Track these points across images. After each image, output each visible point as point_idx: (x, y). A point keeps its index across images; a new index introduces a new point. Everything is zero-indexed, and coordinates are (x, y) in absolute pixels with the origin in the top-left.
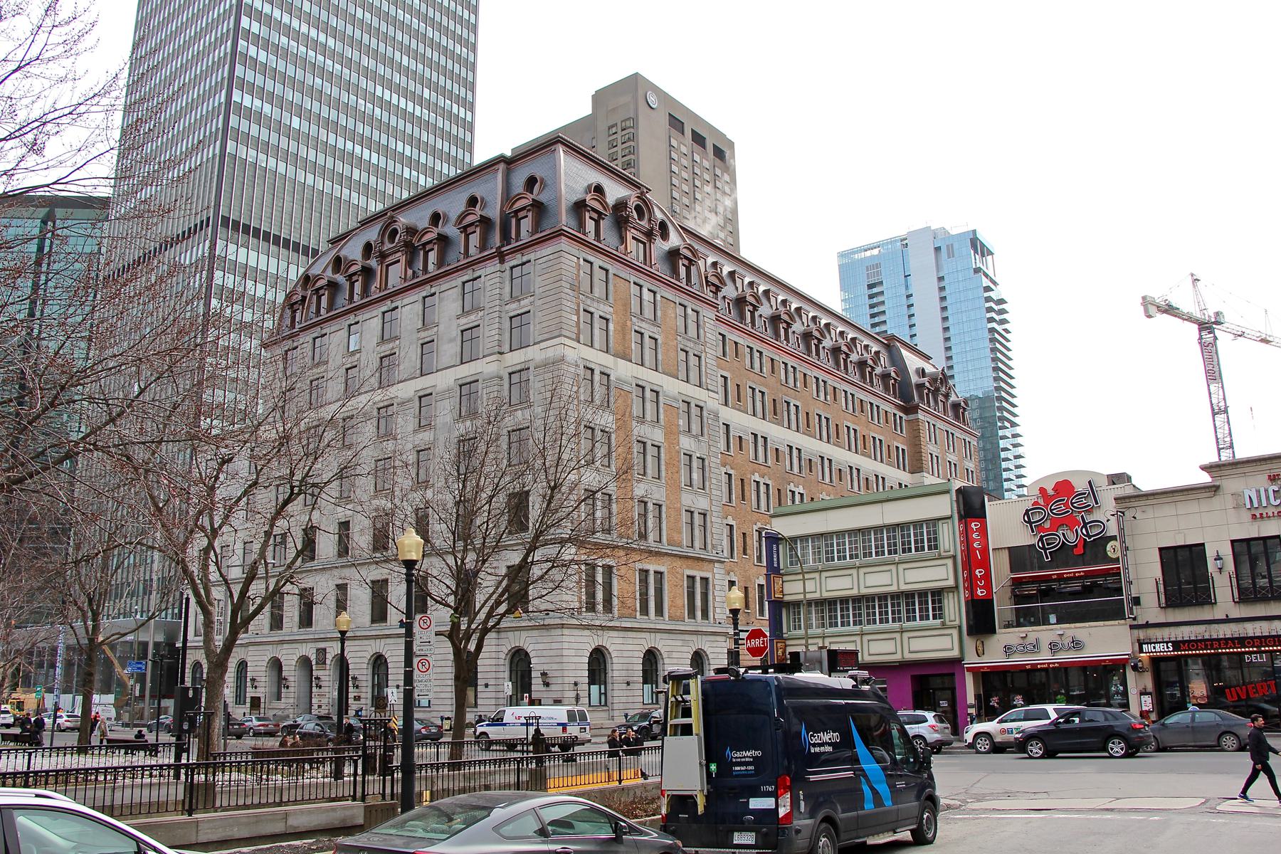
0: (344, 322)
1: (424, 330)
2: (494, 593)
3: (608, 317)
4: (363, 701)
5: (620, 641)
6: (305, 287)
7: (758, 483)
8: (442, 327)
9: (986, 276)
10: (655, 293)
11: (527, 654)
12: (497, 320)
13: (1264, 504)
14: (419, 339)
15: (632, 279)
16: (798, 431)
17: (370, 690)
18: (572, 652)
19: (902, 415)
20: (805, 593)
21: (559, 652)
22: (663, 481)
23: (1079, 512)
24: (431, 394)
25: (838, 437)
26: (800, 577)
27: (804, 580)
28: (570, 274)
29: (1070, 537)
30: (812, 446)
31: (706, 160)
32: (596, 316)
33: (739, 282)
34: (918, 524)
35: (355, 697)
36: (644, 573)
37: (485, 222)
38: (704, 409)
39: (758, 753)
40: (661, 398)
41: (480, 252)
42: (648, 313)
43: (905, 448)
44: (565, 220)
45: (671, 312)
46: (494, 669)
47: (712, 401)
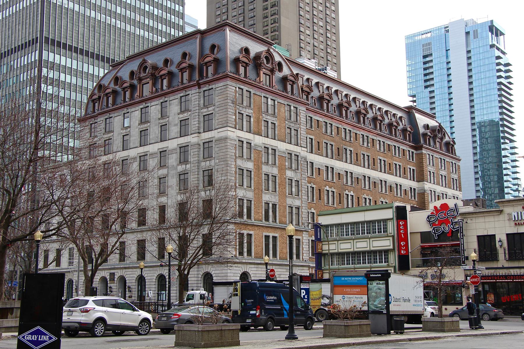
1: (162, 119)
3: (250, 115)
4: (133, 298)
5: (255, 269)
6: (99, 90)
7: (328, 191)
8: (171, 118)
9: (498, 49)
10: (274, 101)
11: (211, 275)
12: (197, 125)
13: (520, 219)
14: (159, 123)
15: (263, 95)
17: (136, 293)
18: (232, 275)
19: (413, 151)
22: (277, 193)
23: (451, 218)
24: (166, 151)
25: (374, 165)
29: (447, 228)
30: (358, 170)
32: (245, 115)
33: (321, 88)
34: (379, 221)
36: (267, 237)
37: (191, 67)
38: (299, 156)
39: (253, 301)
40: (277, 153)
41: (189, 82)
42: (270, 111)
43: (414, 168)
44: (229, 68)
45: (282, 110)
47: (302, 152)
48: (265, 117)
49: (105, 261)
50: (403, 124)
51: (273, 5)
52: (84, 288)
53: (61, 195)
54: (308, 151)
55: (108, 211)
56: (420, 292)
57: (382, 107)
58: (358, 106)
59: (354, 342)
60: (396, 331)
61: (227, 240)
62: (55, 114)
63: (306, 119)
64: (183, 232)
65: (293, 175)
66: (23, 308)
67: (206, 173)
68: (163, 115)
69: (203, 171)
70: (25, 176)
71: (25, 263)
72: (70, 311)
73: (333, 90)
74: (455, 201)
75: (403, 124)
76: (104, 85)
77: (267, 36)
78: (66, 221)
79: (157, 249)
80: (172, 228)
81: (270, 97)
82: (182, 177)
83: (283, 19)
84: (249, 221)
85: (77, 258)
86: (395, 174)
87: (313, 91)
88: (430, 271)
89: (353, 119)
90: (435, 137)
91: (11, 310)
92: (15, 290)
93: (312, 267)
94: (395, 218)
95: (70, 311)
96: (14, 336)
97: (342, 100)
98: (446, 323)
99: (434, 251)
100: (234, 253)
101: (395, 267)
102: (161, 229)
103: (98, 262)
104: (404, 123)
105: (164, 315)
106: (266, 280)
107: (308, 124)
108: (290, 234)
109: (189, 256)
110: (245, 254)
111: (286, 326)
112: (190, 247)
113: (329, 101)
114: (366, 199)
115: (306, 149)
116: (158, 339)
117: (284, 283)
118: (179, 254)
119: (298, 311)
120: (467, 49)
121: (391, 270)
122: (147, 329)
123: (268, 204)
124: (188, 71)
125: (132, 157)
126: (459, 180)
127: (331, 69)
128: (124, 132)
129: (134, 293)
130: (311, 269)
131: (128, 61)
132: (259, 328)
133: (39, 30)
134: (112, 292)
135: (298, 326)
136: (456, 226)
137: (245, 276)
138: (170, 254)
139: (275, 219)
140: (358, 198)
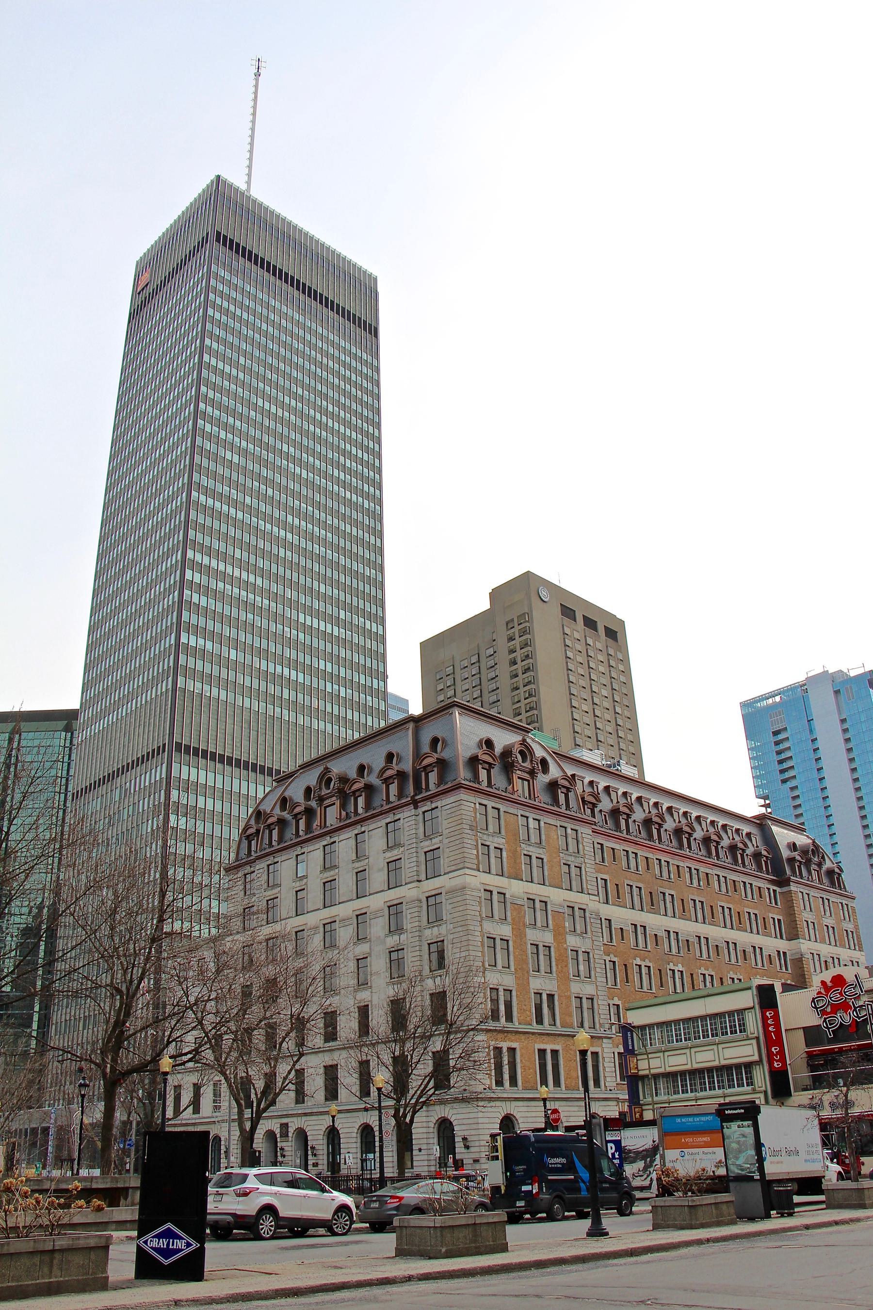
0: (293, 853)
1: (357, 862)
2: (418, 1090)
3: (501, 847)
4: (320, 1167)
5: (525, 1109)
6: (257, 821)
7: (640, 966)
11: (451, 1123)
12: (415, 859)
14: (354, 868)
15: (520, 812)
16: (674, 917)
17: (325, 1157)
18: (486, 1120)
19: (775, 888)
20: (650, 1069)
21: (475, 1121)
22: (555, 975)
23: (851, 999)
24: (366, 913)
26: (646, 1057)
27: (648, 1059)
28: (469, 818)
29: (845, 1018)
30: (687, 928)
31: (600, 641)
32: (492, 848)
33: (613, 795)
34: (731, 1013)
35: (313, 1163)
36: (542, 1052)
37: (401, 775)
38: (587, 911)
39: (525, 1167)
42: (534, 838)
43: (780, 917)
44: (463, 774)
45: (553, 835)
46: (425, 1136)
47: (592, 903)
48: (525, 849)
49: (273, 1103)
50: (753, 845)
51: (525, 670)
52: (239, 1151)
53: (200, 995)
54: (602, 901)
55: (276, 1019)
56: (815, 1135)
57: (715, 819)
58: (677, 821)
59: (708, 1236)
60: (779, 1211)
61: (475, 1061)
62: (191, 861)
63: (594, 848)
64: (400, 1050)
65: (578, 943)
66: (144, 1188)
67: (434, 948)
68: (359, 856)
69: (429, 944)
70: (145, 965)
71: (145, 1109)
72: (218, 1194)
73: (634, 797)
74: (854, 970)
75: (753, 845)
76: (265, 812)
77: (519, 718)
78: (208, 1037)
79: (358, 1083)
80: (380, 1043)
81: (531, 816)
82: (394, 956)
83: (543, 690)
84: (509, 1025)
85: (227, 1098)
86: (749, 930)
87: (601, 802)
88: (828, 1096)
89: (671, 842)
90: (808, 863)
91: (124, 1192)
92: (129, 1156)
93: (624, 1101)
94: (757, 1007)
95: (218, 1194)
96: (130, 1238)
97: (650, 812)
98: (866, 1192)
99: (830, 1059)
100: (488, 1082)
101: (765, 1092)
102: (361, 1046)
103: (262, 1107)
104: (756, 843)
105: (374, 1199)
106: (545, 1130)
107: (596, 856)
108: (582, 1048)
109: (412, 1092)
110: (507, 1083)
111: (585, 1210)
112: (412, 1076)
113: (628, 816)
114: (704, 975)
115: (597, 898)
116: (366, 1242)
117: (577, 1133)
118: (394, 1089)
119: (606, 1182)
120: (839, 717)
121: (760, 1099)
122: (346, 1225)
123: (541, 994)
124: (396, 781)
125: (312, 927)
126: (856, 932)
127: (627, 763)
128: (298, 885)
129: (321, 1157)
130: (620, 1104)
131: (301, 771)
132: (540, 1215)
133: (168, 732)
134: (284, 1156)
135: (607, 1209)
136: (861, 1012)
137: (507, 1122)
138: (379, 1089)
139: (554, 1020)
140: (692, 975)
